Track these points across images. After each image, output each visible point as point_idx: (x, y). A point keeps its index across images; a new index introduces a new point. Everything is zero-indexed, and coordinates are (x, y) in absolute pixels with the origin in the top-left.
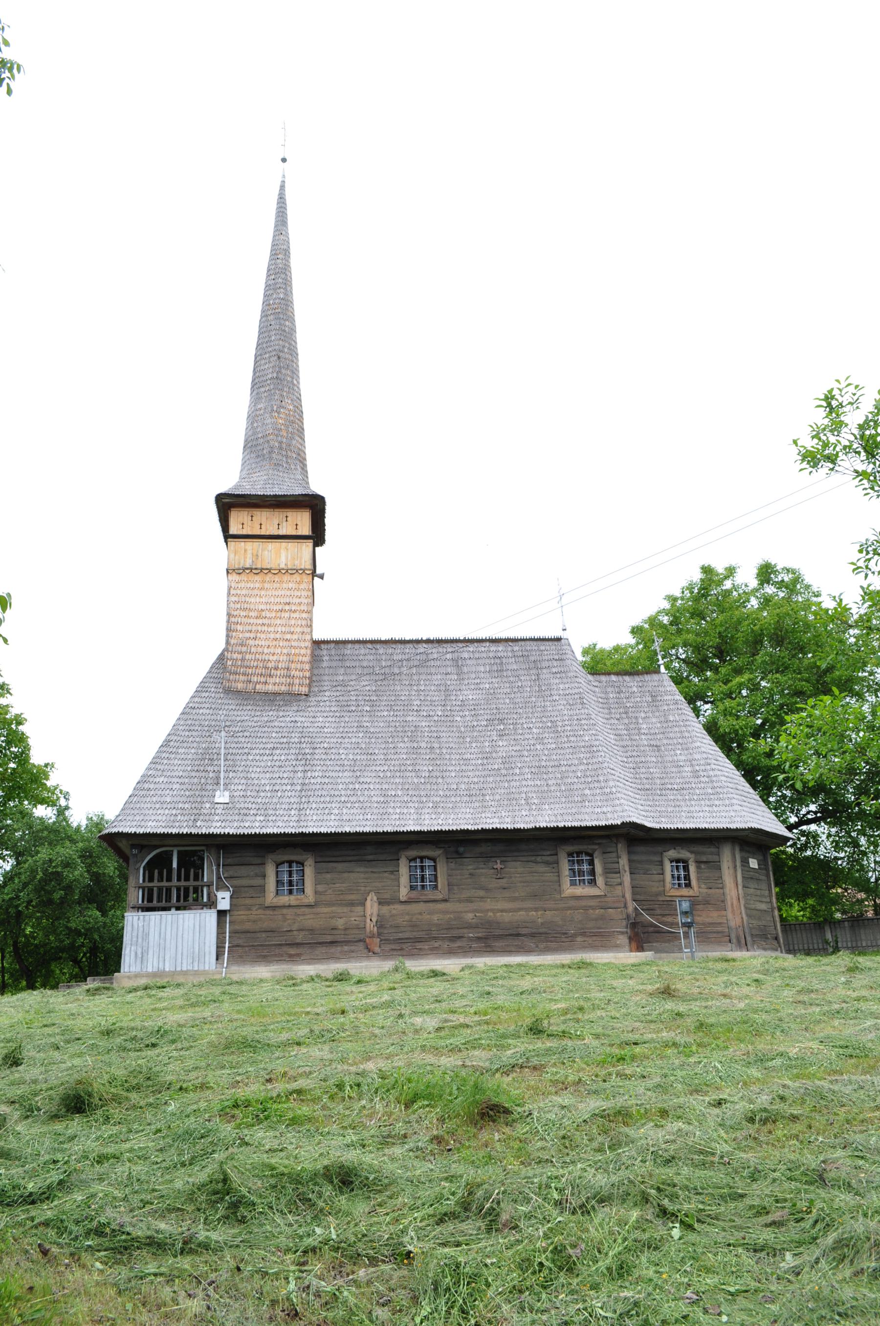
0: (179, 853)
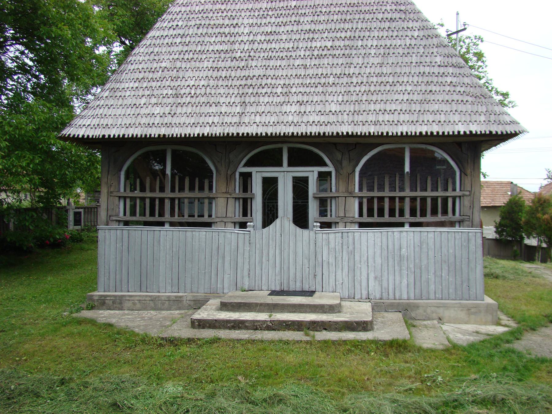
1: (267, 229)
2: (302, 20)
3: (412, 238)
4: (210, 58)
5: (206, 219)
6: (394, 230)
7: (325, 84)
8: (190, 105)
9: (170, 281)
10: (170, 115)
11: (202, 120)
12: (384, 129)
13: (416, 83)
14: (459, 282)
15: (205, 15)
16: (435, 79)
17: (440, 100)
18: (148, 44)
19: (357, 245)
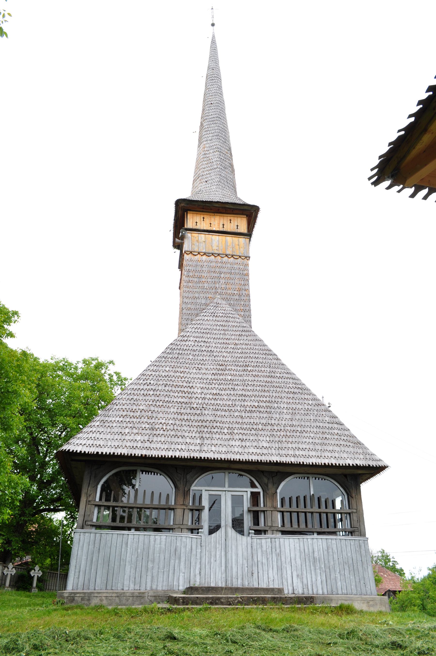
1: (213, 535)
2: (236, 388)
3: (321, 544)
4: (175, 406)
6: (308, 537)
7: (256, 429)
8: (163, 436)
9: (133, 579)
10: (149, 442)
11: (173, 446)
12: (301, 460)
13: (315, 432)
14: (357, 580)
15: (169, 379)
16: (327, 431)
17: (333, 444)
18: (129, 393)
19: (283, 549)
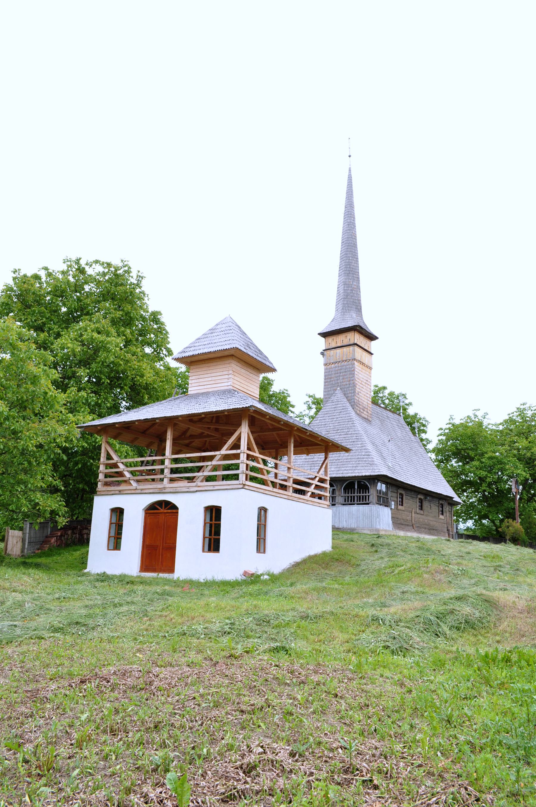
0: (358, 482)
5: (367, 502)
